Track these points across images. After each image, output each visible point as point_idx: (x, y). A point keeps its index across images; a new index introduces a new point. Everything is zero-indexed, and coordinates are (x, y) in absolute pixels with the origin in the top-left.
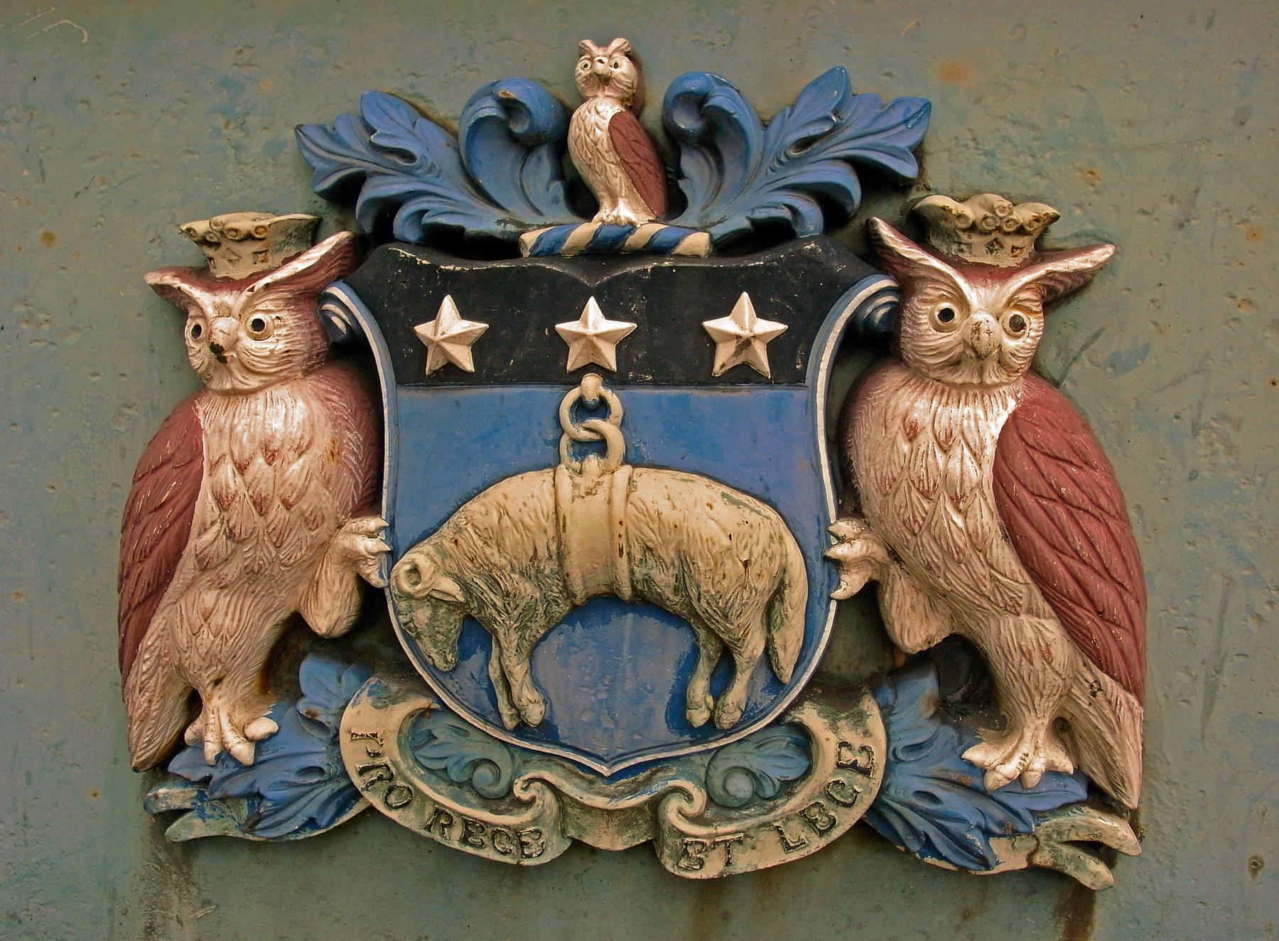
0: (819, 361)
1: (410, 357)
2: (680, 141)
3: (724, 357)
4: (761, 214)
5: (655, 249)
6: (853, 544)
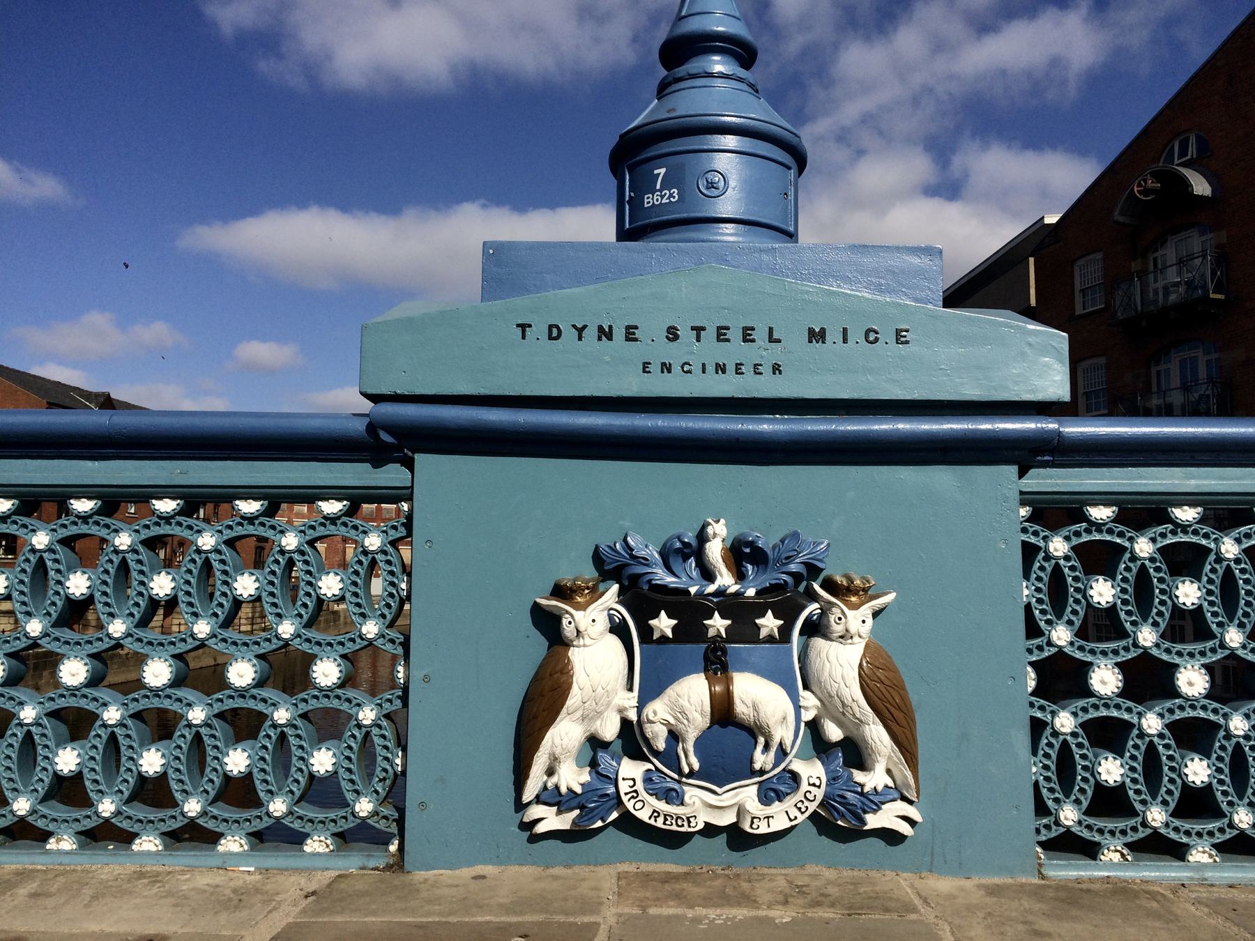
0: (1206, 478)
1: (646, 633)
2: (743, 554)
3: (763, 633)
4: (774, 582)
5: (738, 594)
6: (809, 700)
